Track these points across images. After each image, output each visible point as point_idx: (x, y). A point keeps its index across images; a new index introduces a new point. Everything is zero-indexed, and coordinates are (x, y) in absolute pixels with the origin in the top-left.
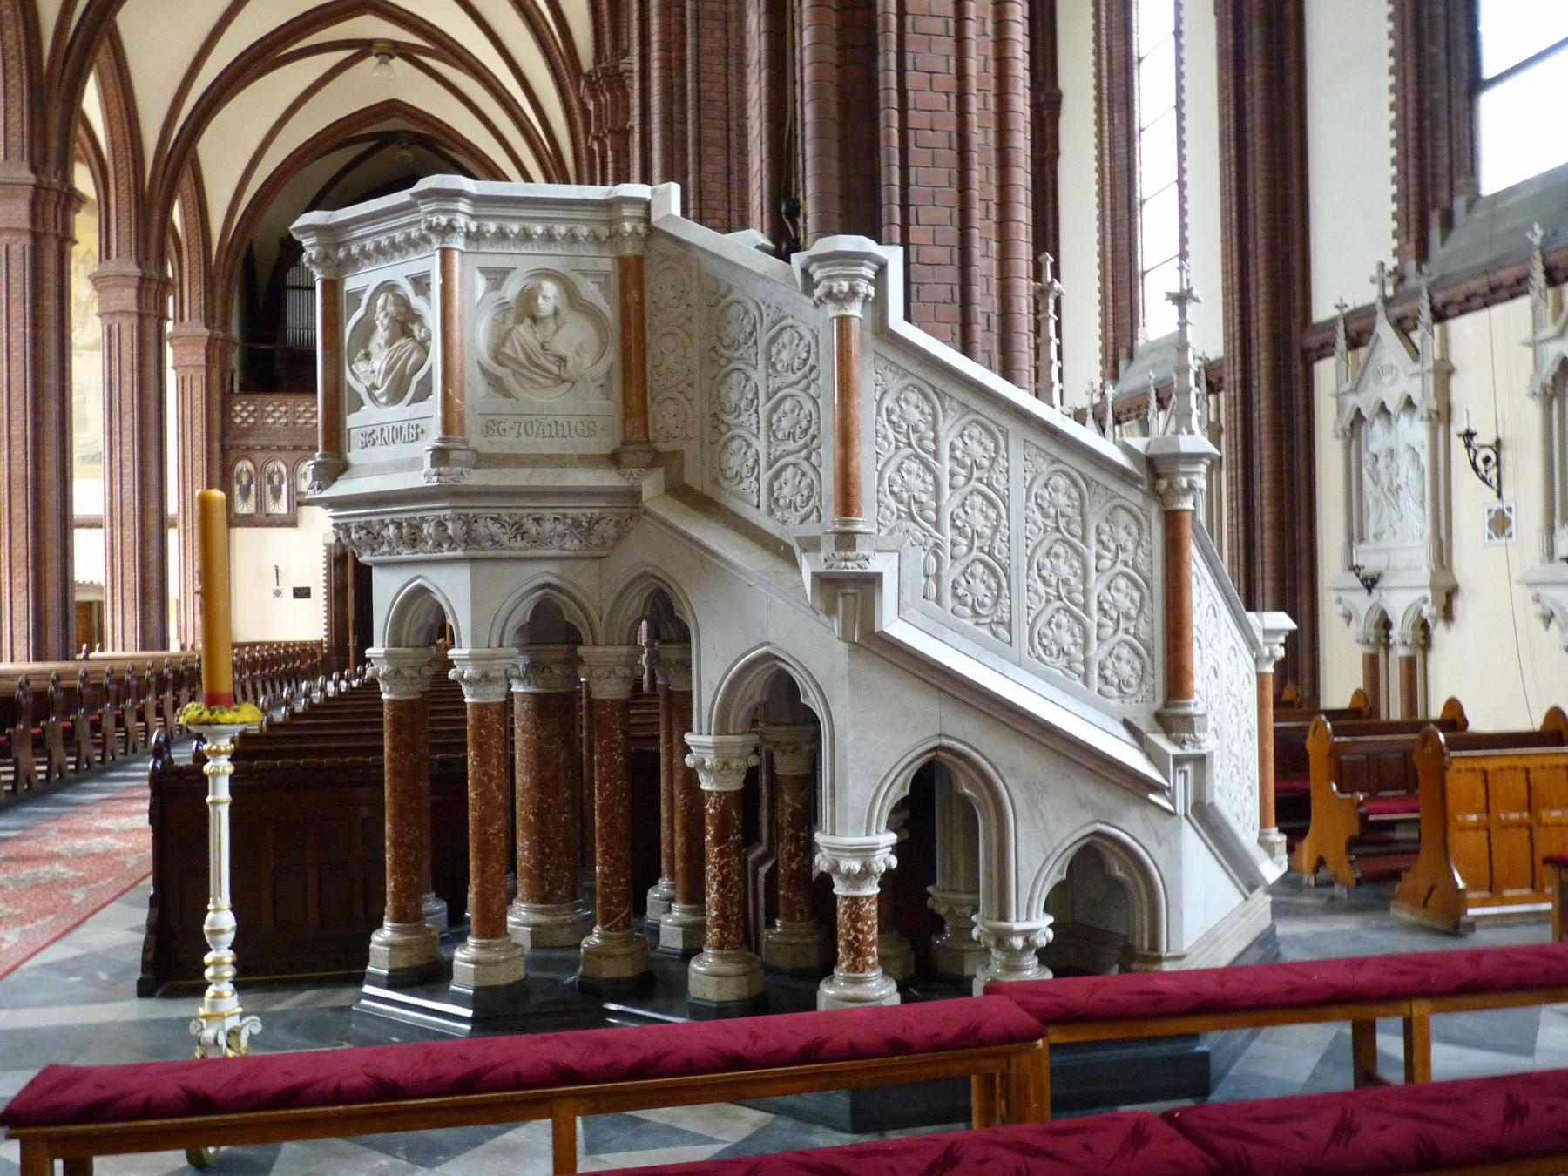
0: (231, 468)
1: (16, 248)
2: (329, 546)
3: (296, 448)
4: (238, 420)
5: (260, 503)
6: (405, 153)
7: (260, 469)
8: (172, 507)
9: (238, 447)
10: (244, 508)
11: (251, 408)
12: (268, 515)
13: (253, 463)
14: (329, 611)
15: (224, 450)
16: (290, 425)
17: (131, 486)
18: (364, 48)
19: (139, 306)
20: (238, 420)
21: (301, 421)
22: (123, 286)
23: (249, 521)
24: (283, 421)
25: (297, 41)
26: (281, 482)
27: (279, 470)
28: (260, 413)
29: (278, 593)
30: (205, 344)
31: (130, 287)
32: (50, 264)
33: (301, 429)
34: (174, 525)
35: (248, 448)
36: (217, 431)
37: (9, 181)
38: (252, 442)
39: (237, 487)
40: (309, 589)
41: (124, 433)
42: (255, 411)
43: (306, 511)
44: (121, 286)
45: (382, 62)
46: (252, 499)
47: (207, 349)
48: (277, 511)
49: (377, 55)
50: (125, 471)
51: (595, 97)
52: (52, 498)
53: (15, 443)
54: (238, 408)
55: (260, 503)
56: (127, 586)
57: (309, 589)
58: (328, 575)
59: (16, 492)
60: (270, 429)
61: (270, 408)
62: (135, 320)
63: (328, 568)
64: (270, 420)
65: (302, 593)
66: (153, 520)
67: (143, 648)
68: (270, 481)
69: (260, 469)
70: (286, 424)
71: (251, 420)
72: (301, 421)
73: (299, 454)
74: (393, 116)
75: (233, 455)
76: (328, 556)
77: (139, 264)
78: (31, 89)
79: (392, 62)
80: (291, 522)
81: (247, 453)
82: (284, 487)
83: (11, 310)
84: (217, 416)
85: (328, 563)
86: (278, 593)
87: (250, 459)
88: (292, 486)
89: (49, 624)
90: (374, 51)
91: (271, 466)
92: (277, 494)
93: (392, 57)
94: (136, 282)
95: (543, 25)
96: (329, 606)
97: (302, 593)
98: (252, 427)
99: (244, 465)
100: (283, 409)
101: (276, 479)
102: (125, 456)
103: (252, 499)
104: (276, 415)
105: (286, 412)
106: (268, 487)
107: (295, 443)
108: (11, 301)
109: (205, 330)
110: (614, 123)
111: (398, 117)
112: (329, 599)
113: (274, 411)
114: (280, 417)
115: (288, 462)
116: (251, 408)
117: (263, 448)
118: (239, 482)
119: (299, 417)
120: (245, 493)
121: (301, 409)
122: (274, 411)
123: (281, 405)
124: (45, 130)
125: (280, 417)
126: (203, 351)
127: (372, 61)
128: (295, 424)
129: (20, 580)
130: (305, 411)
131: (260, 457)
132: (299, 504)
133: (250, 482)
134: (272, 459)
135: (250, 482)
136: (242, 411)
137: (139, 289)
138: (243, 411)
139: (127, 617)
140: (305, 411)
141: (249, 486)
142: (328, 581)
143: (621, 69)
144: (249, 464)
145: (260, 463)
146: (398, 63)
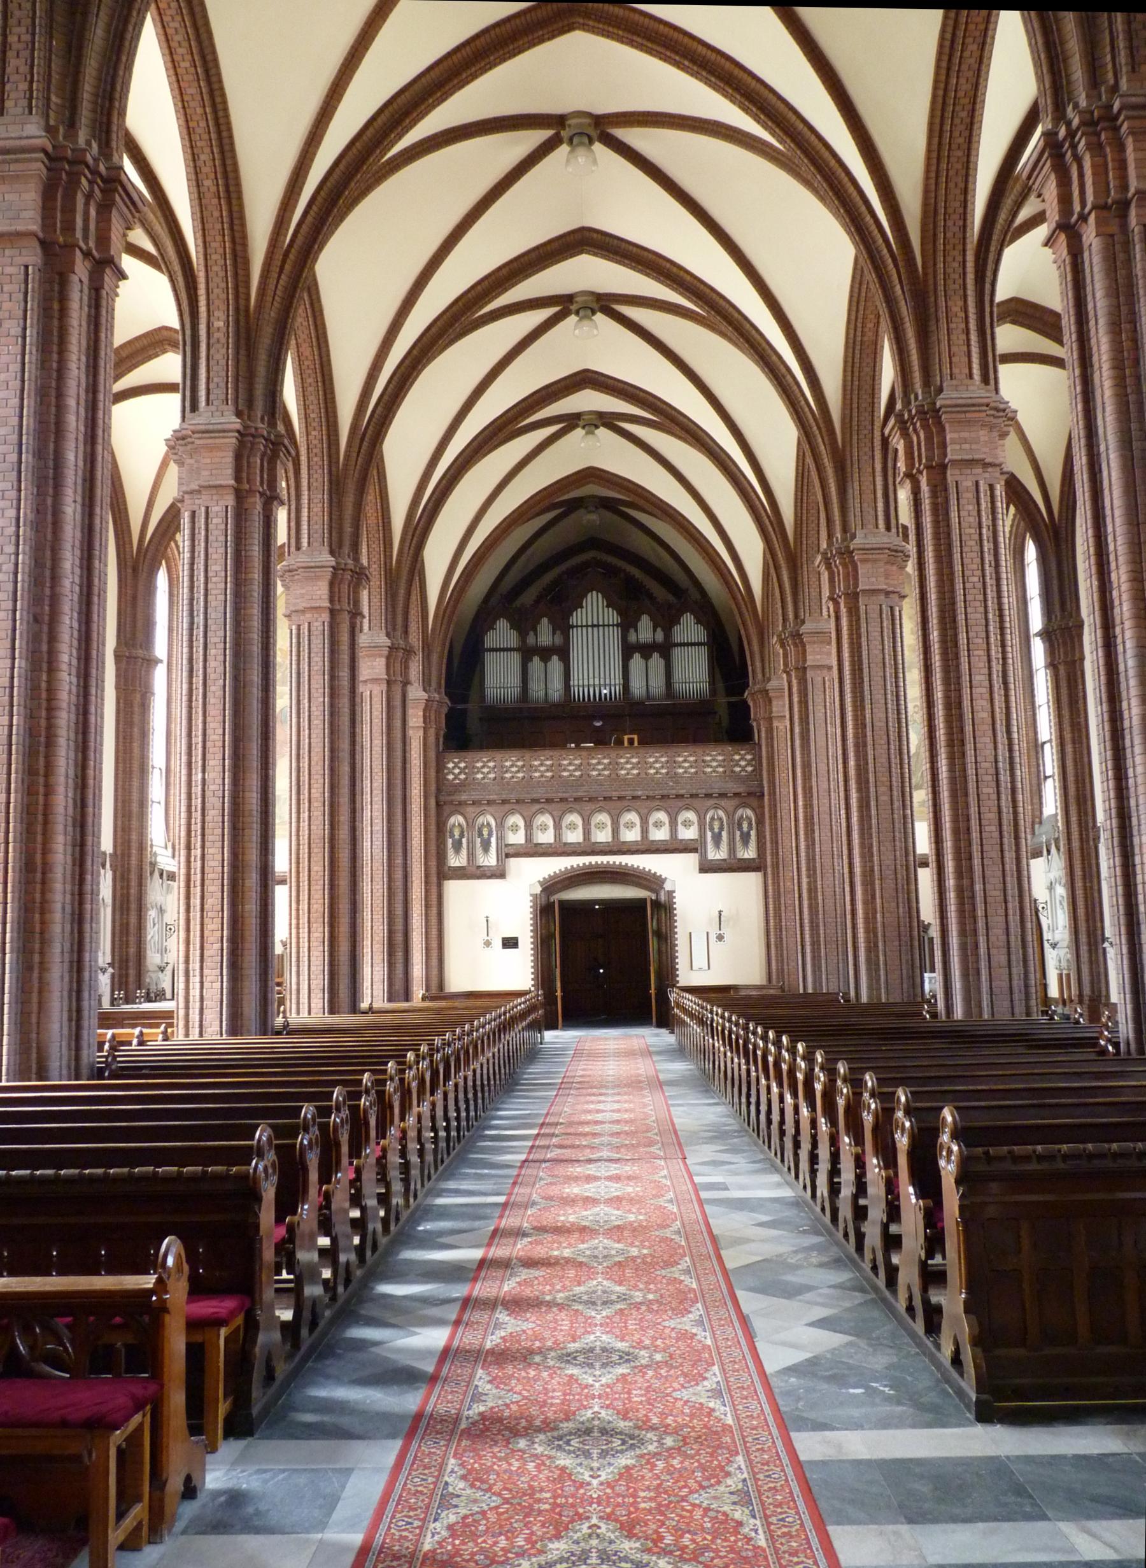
0: (445, 823)
1: (317, 626)
2: (535, 896)
3: (504, 802)
4: (451, 777)
5: (471, 856)
6: (593, 517)
7: (470, 824)
8: (281, 862)
9: (451, 802)
10: (456, 860)
11: (462, 765)
12: (479, 867)
13: (465, 818)
14: (535, 961)
15: (438, 805)
16: (613, 776)
17: (380, 843)
18: (571, 421)
19: (388, 674)
20: (451, 777)
21: (508, 775)
22: (374, 656)
23: (462, 874)
24: (492, 776)
25: (525, 418)
26: (490, 835)
27: (489, 824)
28: (471, 769)
29: (488, 944)
30: (423, 706)
31: (380, 656)
32: (345, 638)
33: (508, 784)
34: (283, 882)
35: (460, 803)
36: (433, 788)
37: (313, 564)
38: (464, 797)
39: (450, 841)
40: (516, 939)
41: (375, 792)
42: (466, 767)
43: (514, 864)
44: (372, 656)
45: (587, 433)
46: (464, 852)
47: (425, 711)
48: (486, 863)
49: (583, 427)
50: (375, 828)
51: (905, 434)
52: (252, 856)
53: (315, 804)
54: (451, 765)
55: (471, 856)
56: (376, 938)
57: (516, 939)
58: (535, 925)
59: (315, 850)
60: (479, 784)
61: (479, 765)
62: (384, 687)
63: (534, 918)
64: (480, 776)
65: (510, 943)
66: (252, 880)
67: (390, 1000)
68: (480, 834)
69: (470, 824)
70: (495, 778)
71: (462, 776)
72: (508, 775)
73: (507, 807)
74: (588, 483)
75: (447, 809)
76: (534, 907)
77: (388, 635)
78: (330, 482)
79: (597, 431)
80: (499, 873)
81: (459, 807)
82: (493, 840)
83: (312, 681)
84: (432, 773)
85: (534, 913)
86: (488, 944)
87: (462, 814)
88: (501, 839)
89: (341, 977)
90: (581, 423)
91: (481, 820)
92: (486, 847)
93: (597, 427)
94: (385, 652)
95: (789, 377)
96: (535, 955)
97: (510, 943)
98: (463, 784)
99: (457, 820)
100: (491, 764)
101: (485, 832)
102: (375, 814)
103: (464, 852)
104: (485, 770)
105: (495, 767)
106: (479, 840)
107: (504, 797)
108: (312, 673)
109: (424, 694)
110: (930, 458)
111: (594, 483)
112: (535, 949)
113: (483, 767)
114: (489, 773)
115: (497, 815)
116: (462, 765)
117: (474, 803)
118: (452, 836)
119: (506, 772)
120: (457, 847)
121: (508, 764)
122: (483, 767)
123: (489, 761)
124: (341, 518)
125: (489, 773)
126: (421, 713)
127: (579, 432)
128: (503, 778)
129: (317, 935)
130: (512, 766)
131: (470, 810)
132: (508, 856)
133: (462, 835)
134: (482, 813)
135: (462, 835)
136: (454, 768)
137: (388, 658)
138: (456, 767)
139: (376, 969)
140: (512, 766)
141: (720, 833)
142: (535, 931)
143: (938, 405)
144: (460, 819)
145: (471, 816)
146: (602, 432)
